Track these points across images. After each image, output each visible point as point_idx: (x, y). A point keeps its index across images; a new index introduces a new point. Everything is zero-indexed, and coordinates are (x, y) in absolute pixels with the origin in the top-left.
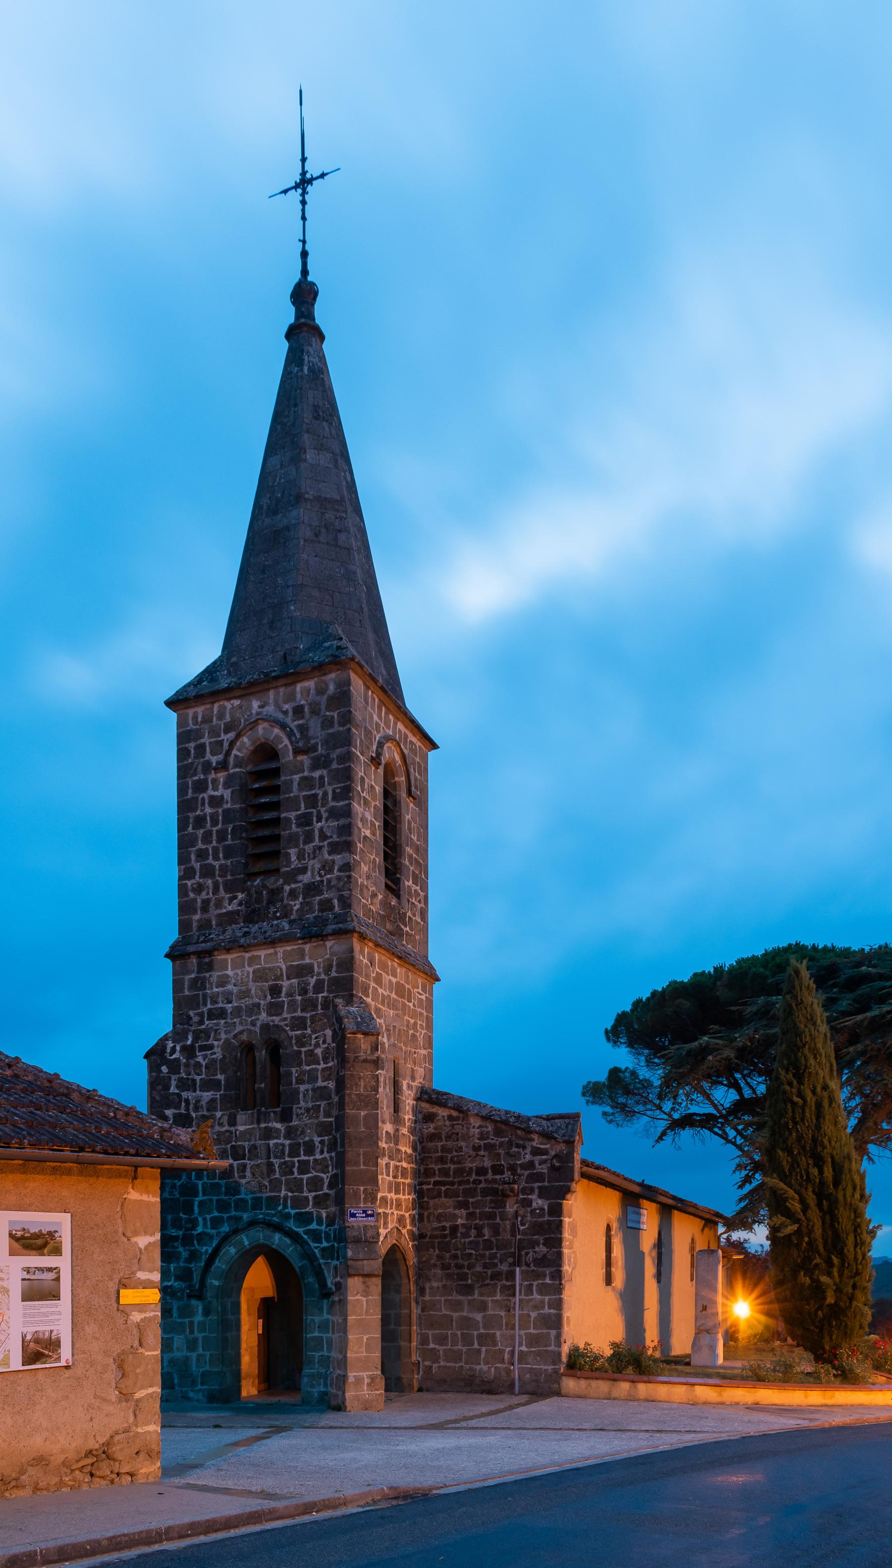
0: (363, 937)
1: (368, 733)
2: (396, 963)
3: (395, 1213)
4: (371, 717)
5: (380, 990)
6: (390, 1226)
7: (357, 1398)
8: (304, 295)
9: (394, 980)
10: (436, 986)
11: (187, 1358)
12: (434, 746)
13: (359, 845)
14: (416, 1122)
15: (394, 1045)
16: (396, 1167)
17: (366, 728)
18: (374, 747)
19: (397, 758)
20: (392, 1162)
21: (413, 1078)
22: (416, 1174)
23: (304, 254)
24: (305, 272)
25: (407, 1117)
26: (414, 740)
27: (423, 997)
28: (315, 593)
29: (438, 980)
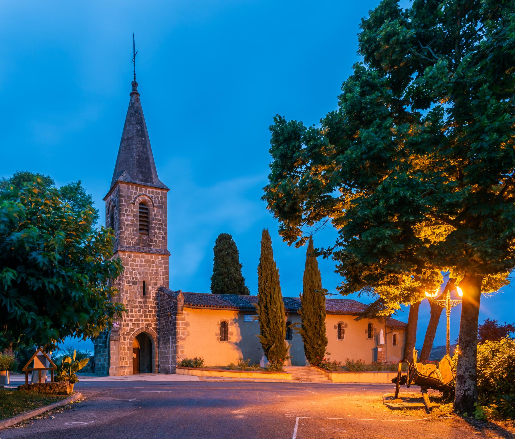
0: (123, 251)
1: (130, 197)
2: (144, 254)
3: (145, 323)
4: (131, 192)
5: (135, 263)
6: (141, 327)
7: (112, 372)
8: (135, 84)
9: (143, 259)
10: (170, 257)
11: (104, 364)
12: (167, 190)
13: (124, 227)
14: (157, 297)
15: (144, 277)
16: (145, 311)
17: (128, 196)
18: (133, 200)
19: (147, 198)
20: (142, 310)
21: (156, 284)
22: (157, 311)
23: (135, 74)
24: (135, 79)
25: (152, 296)
26: (157, 191)
27: (163, 261)
28: (123, 164)
29: (170, 255)
